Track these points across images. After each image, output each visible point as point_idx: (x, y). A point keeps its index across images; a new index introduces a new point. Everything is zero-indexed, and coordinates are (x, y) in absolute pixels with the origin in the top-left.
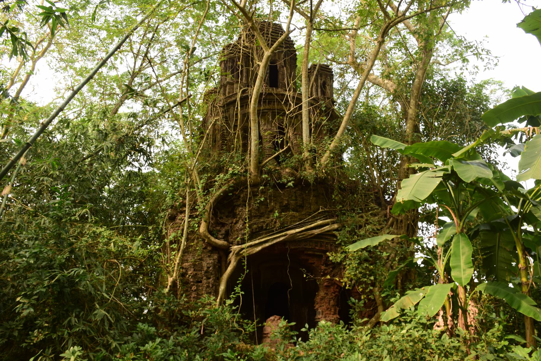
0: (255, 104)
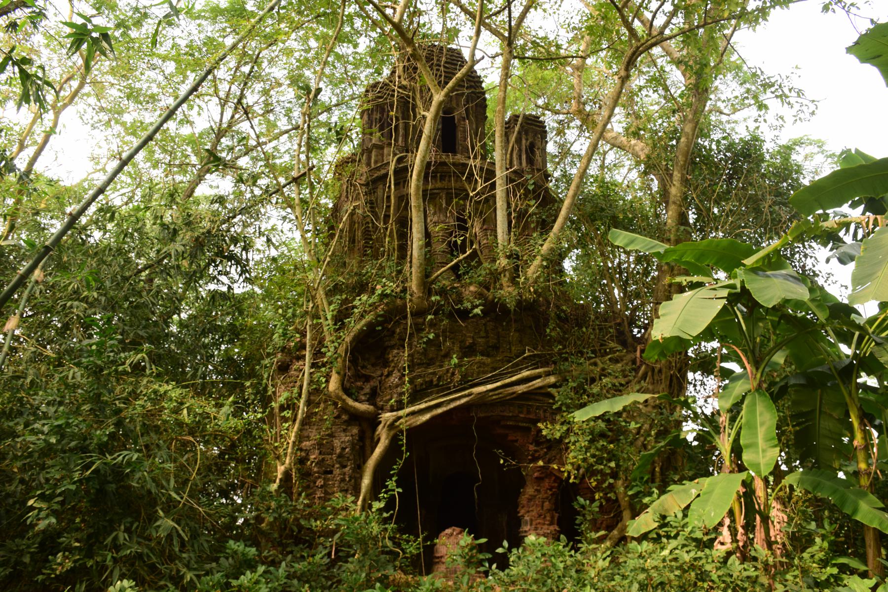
0: (418, 180)
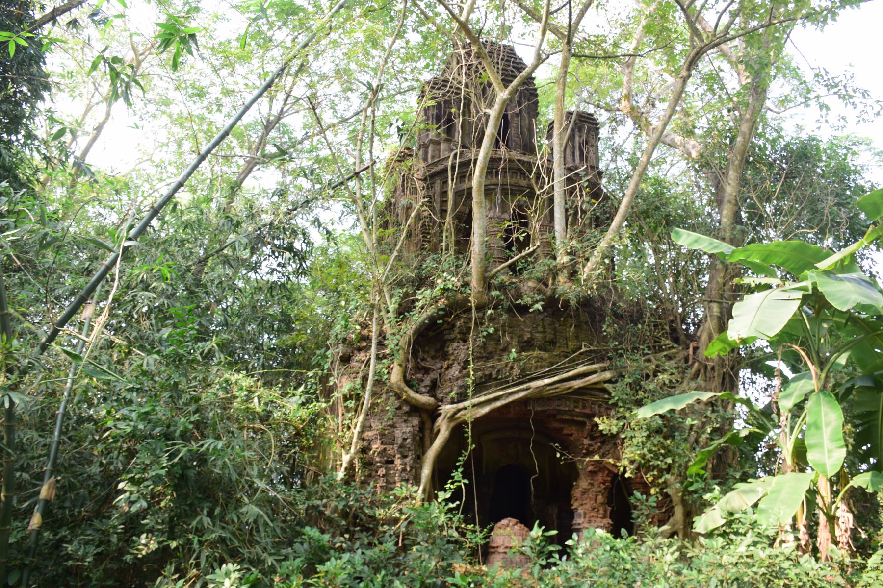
0: (480, 177)
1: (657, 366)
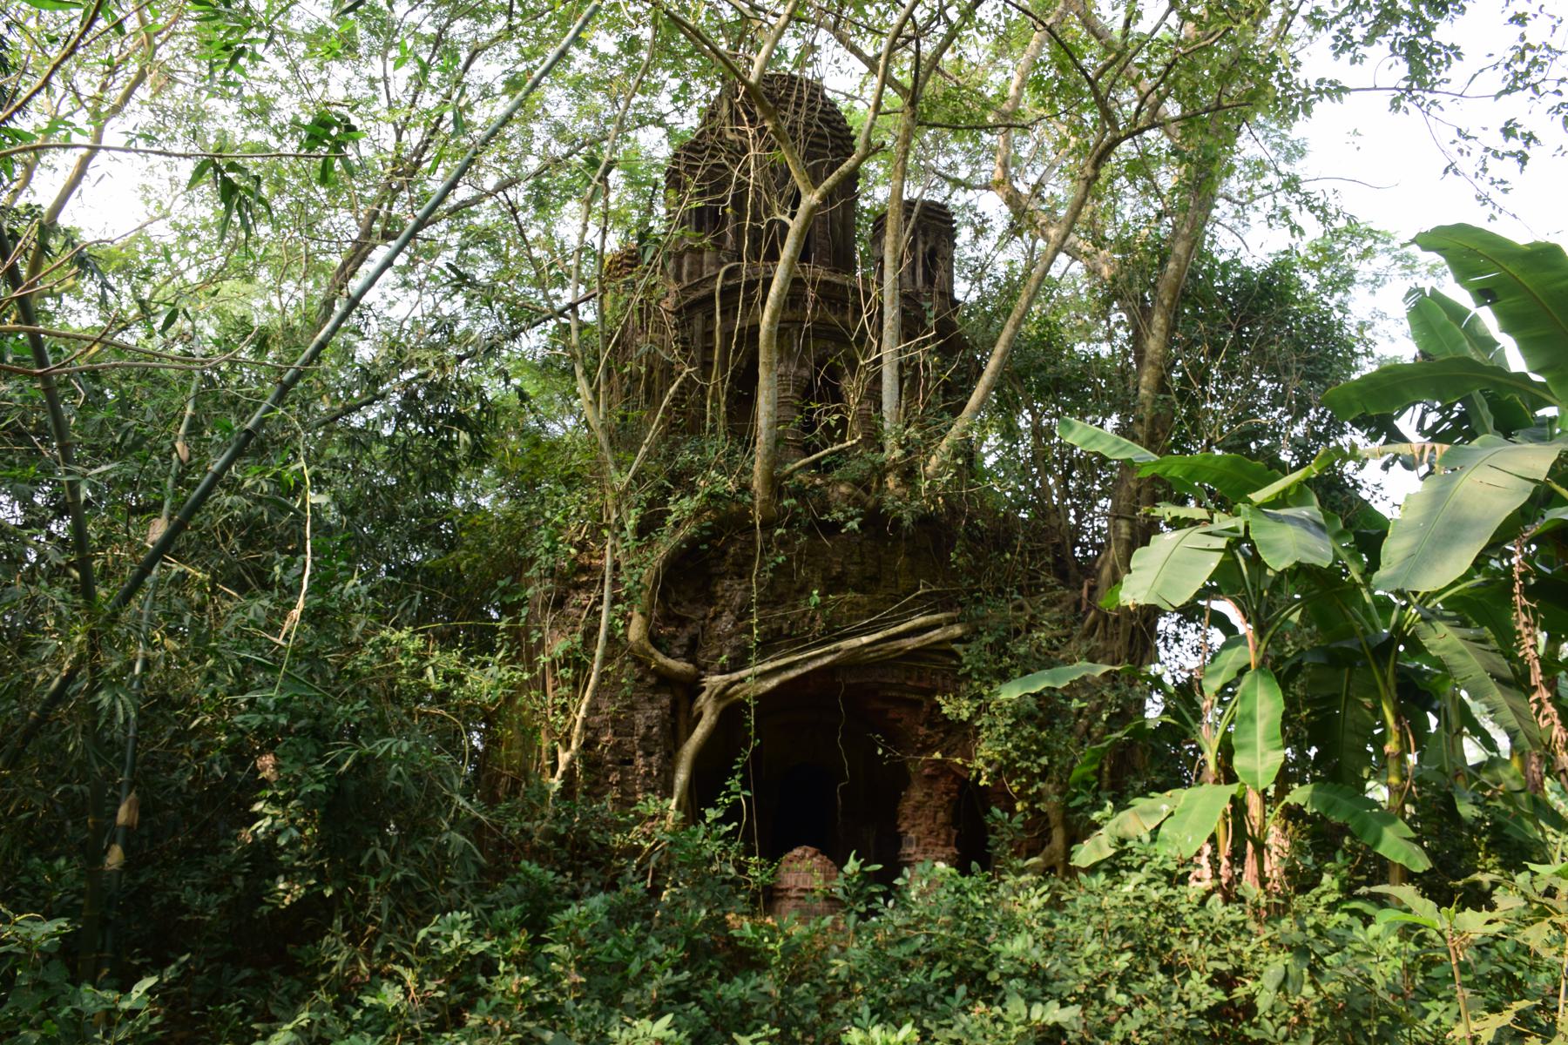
1: (1033, 617)
